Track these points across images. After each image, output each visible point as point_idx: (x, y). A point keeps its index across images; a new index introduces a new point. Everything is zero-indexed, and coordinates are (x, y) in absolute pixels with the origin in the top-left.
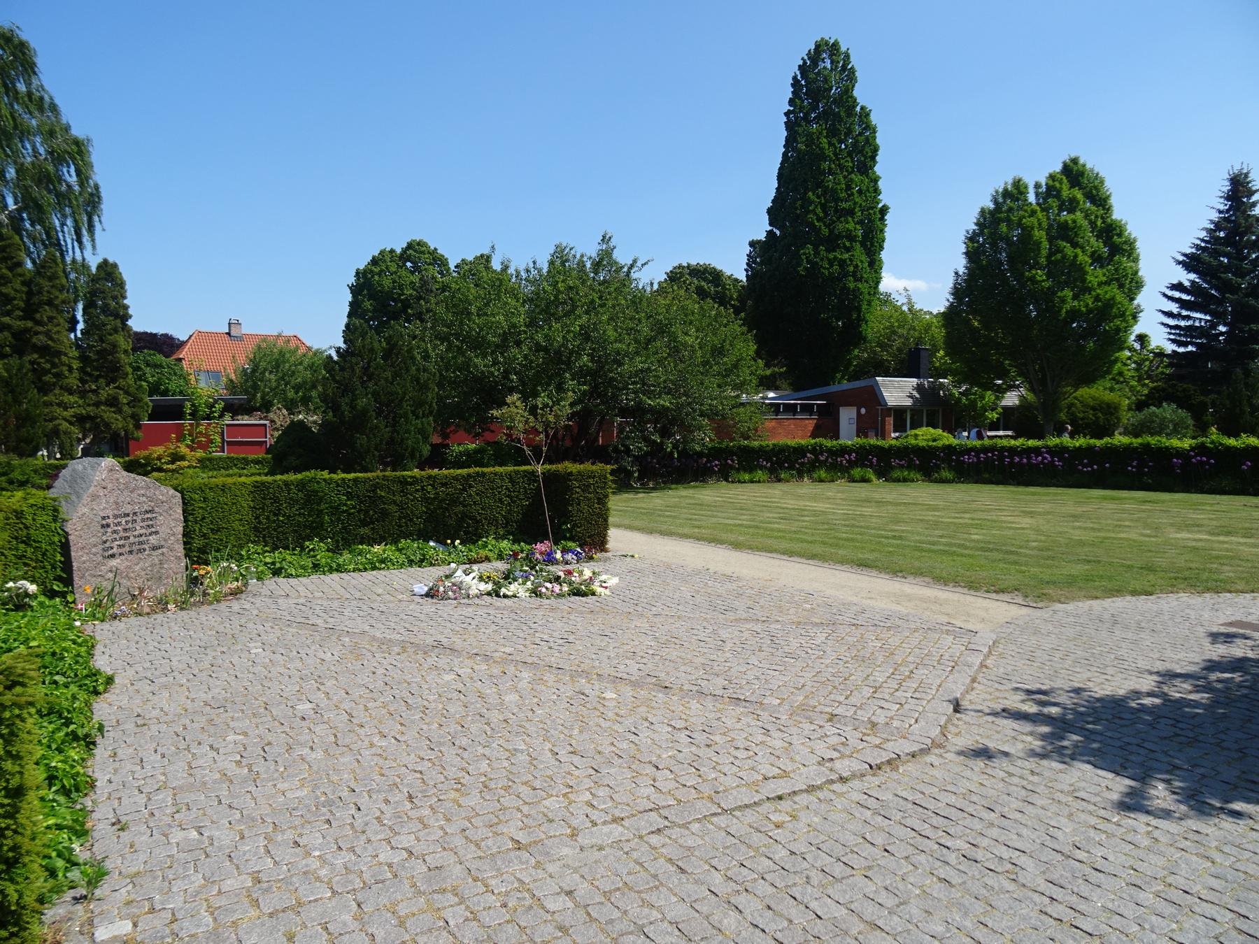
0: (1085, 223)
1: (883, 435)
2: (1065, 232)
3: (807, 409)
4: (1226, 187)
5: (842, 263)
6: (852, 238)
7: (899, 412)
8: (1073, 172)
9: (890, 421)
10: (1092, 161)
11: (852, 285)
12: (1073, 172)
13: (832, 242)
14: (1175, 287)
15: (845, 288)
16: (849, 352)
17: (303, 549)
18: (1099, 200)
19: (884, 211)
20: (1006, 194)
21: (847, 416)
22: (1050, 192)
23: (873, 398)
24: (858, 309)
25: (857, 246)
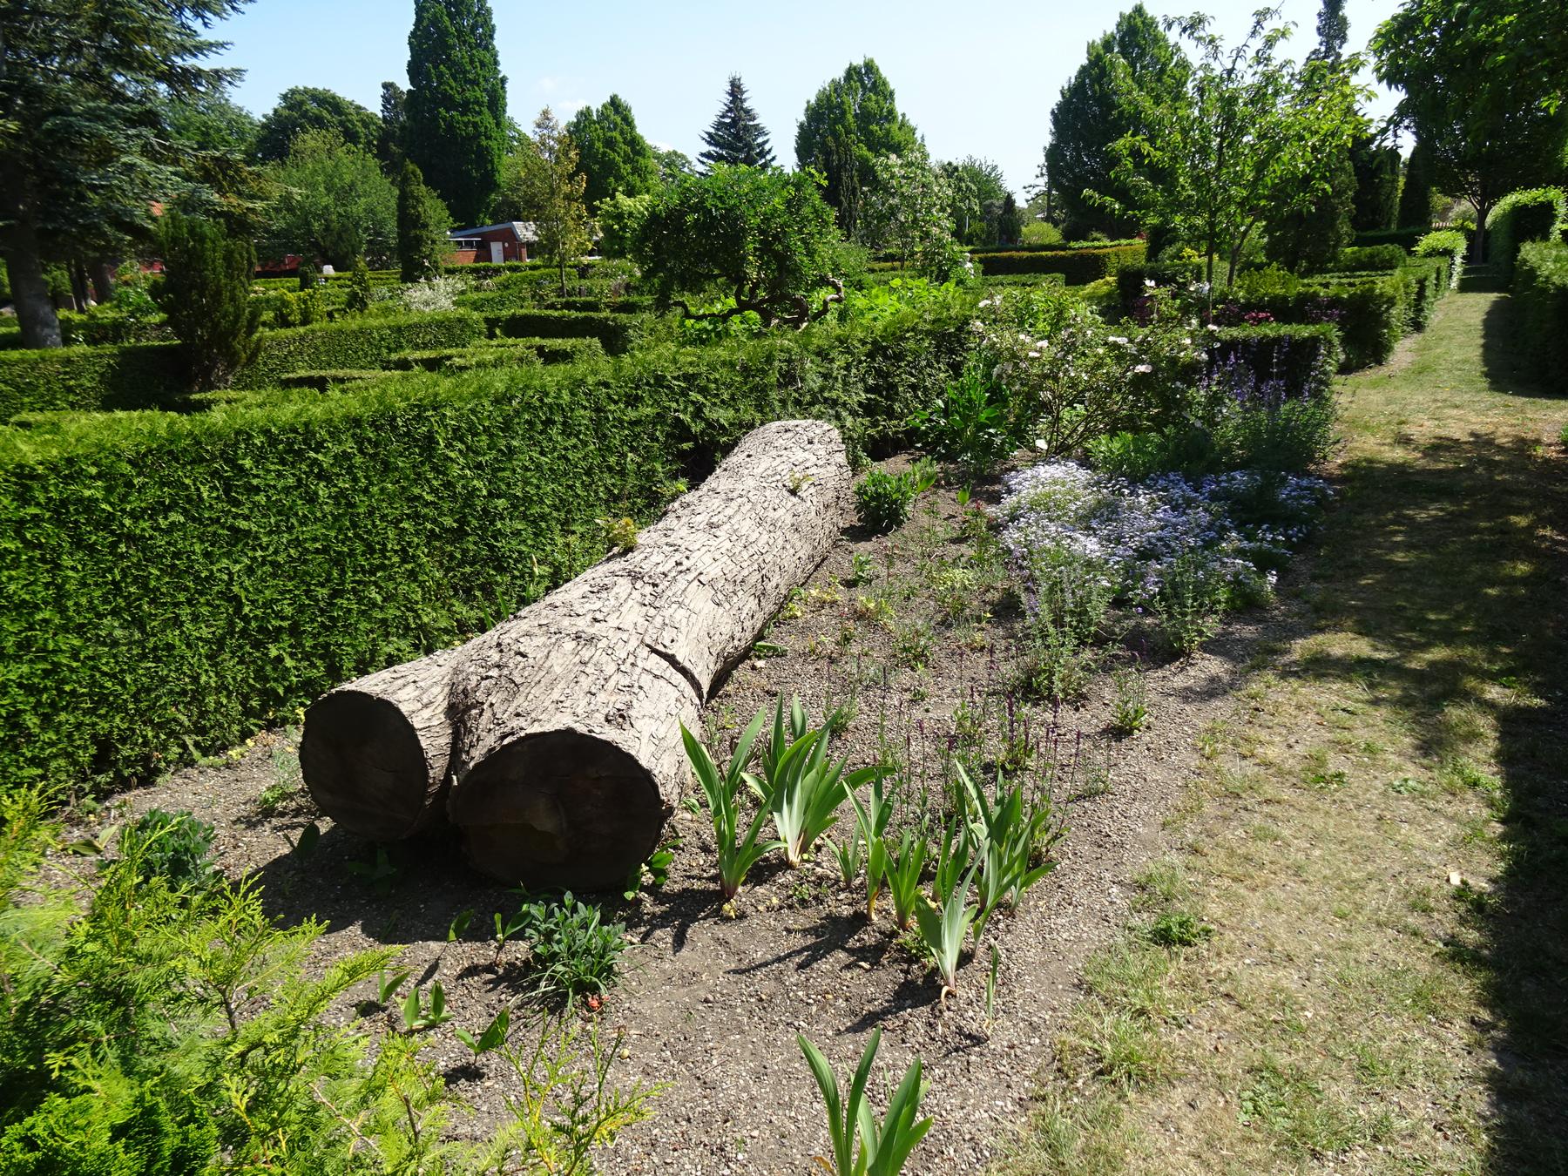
0: (619, 138)
1: (521, 259)
2: (610, 143)
3: (469, 244)
4: (728, 88)
5: (475, 125)
6: (480, 104)
7: (529, 245)
8: (614, 103)
9: (524, 251)
10: (624, 98)
11: (484, 143)
12: (614, 103)
13: (465, 107)
14: (702, 155)
15: (479, 146)
16: (488, 195)
17: (729, 210)
18: (628, 121)
19: (504, 80)
20: (582, 113)
21: (496, 248)
22: (603, 116)
23: (510, 236)
24: (492, 162)
25: (485, 110)
